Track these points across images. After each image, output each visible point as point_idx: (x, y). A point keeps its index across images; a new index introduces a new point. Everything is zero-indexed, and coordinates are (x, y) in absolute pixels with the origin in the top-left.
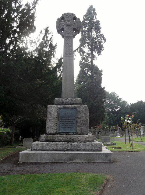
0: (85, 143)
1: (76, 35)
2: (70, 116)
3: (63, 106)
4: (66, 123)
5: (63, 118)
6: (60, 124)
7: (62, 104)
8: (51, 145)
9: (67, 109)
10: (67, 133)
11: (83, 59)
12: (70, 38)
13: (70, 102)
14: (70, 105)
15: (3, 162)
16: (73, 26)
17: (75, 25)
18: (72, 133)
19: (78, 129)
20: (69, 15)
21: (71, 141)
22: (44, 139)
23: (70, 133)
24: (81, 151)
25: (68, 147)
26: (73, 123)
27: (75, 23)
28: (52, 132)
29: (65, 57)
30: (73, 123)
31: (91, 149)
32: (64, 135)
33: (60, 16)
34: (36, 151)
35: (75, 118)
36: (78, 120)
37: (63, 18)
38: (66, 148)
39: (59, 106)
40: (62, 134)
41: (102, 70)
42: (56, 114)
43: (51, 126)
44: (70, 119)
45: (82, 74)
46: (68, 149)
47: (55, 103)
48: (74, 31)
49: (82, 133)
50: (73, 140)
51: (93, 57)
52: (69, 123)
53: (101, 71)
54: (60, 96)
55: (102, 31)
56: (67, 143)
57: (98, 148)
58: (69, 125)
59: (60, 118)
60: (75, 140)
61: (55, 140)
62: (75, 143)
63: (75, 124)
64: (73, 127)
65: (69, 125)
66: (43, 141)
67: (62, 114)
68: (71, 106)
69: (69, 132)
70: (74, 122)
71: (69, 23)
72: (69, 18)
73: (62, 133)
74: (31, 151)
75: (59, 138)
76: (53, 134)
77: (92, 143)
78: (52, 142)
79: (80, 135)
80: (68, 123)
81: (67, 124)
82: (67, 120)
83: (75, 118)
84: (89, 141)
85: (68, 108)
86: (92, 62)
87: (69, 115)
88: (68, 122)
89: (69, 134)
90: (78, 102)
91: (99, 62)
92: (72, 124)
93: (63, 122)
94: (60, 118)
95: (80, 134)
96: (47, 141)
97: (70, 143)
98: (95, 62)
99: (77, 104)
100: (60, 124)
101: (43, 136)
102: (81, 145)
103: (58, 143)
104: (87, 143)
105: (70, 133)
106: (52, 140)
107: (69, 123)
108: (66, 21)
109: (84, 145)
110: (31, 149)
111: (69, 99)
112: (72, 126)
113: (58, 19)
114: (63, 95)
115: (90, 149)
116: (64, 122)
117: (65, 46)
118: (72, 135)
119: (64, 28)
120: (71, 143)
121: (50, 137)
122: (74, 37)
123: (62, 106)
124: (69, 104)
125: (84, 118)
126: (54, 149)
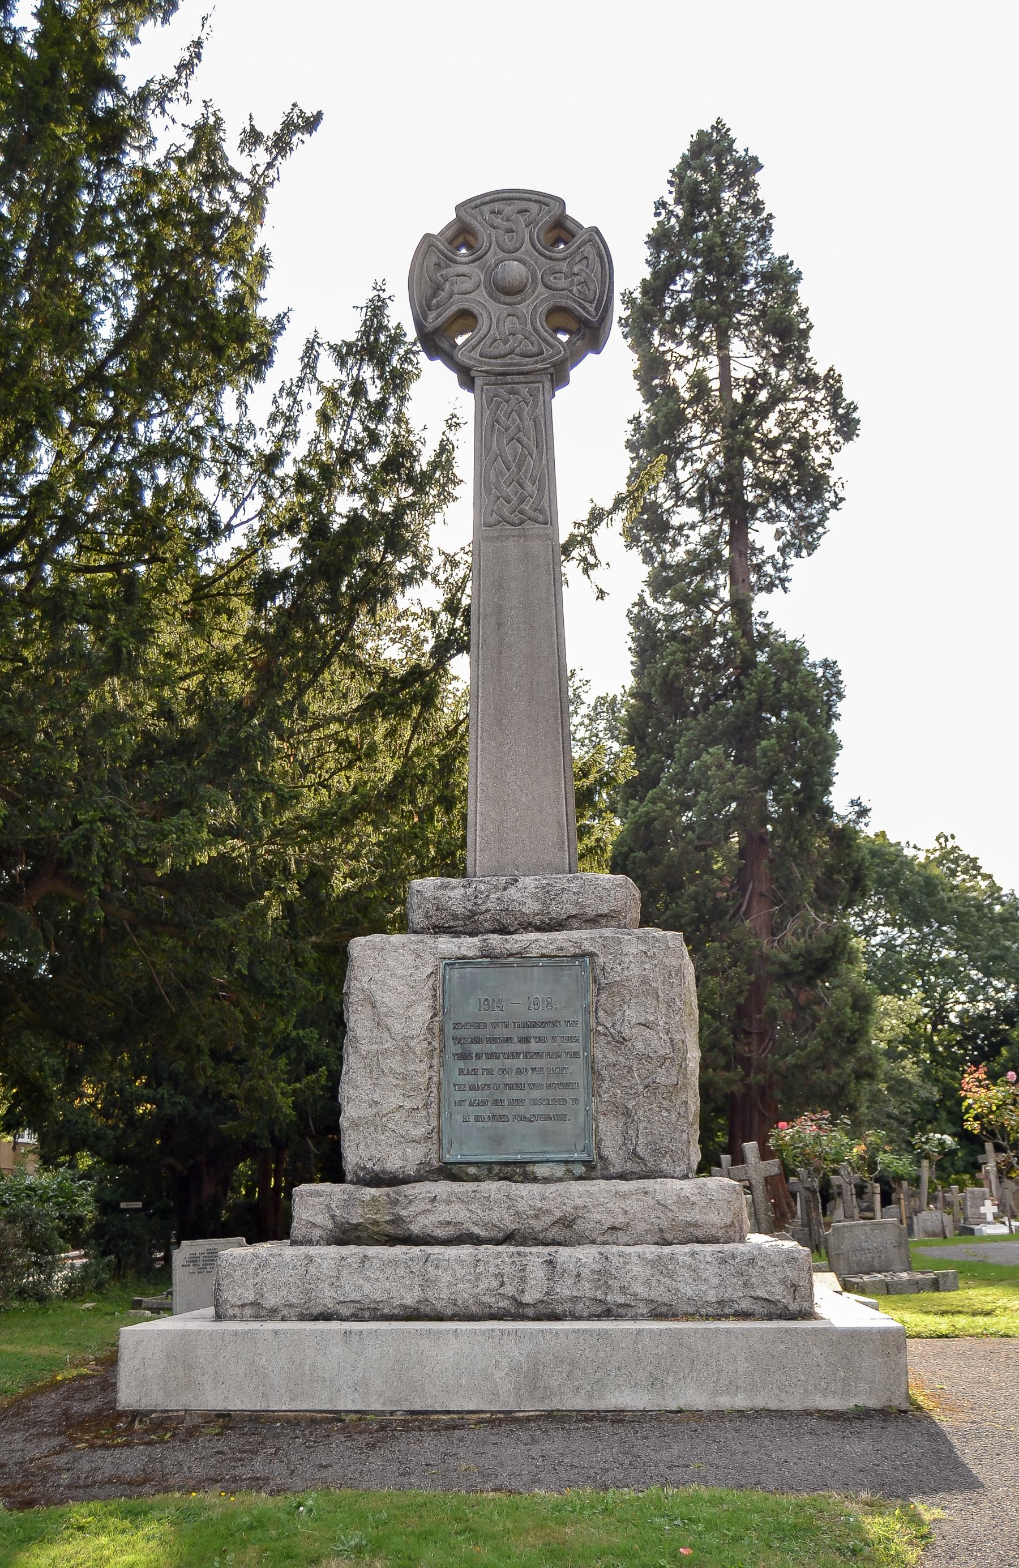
0: (667, 1250)
1: (575, 357)
2: (534, 1025)
3: (476, 940)
4: (511, 1087)
5: (476, 1041)
6: (458, 1096)
7: (465, 925)
8: (383, 1272)
9: (510, 965)
10: (515, 1171)
11: (659, 584)
12: (524, 390)
13: (536, 907)
14: (533, 936)
15: (16, 1411)
16: (547, 293)
17: (563, 283)
18: (559, 1171)
19: (609, 1129)
20: (508, 209)
21: (553, 1233)
22: (318, 1220)
23: (541, 1171)
24: (634, 1318)
25: (523, 1280)
26: (567, 1086)
27: (564, 266)
28: (393, 1164)
29: (487, 539)
30: (567, 1086)
31: (721, 1303)
32: (492, 1188)
33: (439, 218)
34: (256, 1317)
35: (573, 1039)
36: (603, 1052)
37: (462, 233)
38: (509, 1290)
39: (447, 945)
40: (476, 1179)
41: (848, 680)
42: (422, 1012)
43: (381, 1107)
44: (534, 1046)
45: (655, 711)
46: (527, 1299)
47: (417, 918)
48: (557, 330)
49: (636, 1169)
50: (567, 1222)
51: (749, 575)
52: (533, 1086)
53: (951, 856)
54: (450, 862)
55: (821, 354)
56: (512, 1249)
57: (779, 1293)
58: (534, 1102)
59: (458, 1040)
60: (580, 1226)
61: (415, 1228)
62: (586, 1254)
63: (581, 1094)
64: (562, 1117)
65: (534, 1102)
66: (317, 1233)
67: (470, 1010)
68: (544, 936)
69: (535, 1157)
70: (576, 1072)
71: (514, 270)
72: (509, 231)
73: (472, 1170)
74: (219, 1317)
75: (444, 1213)
76: (394, 1180)
77: (726, 1247)
78: (392, 1241)
79: (623, 1186)
80: (519, 1086)
81: (516, 1094)
82: (515, 1055)
83: (573, 1039)
84: (699, 1233)
85: (519, 954)
86: (740, 606)
87: (533, 1016)
88: (521, 1079)
89: (535, 1180)
90: (604, 909)
91: (810, 607)
92: (560, 1093)
93: (482, 1080)
94: (458, 1040)
95: (623, 1177)
96: (345, 1235)
97: (534, 1250)
98: (771, 609)
99: (594, 921)
100: (458, 1096)
101: (313, 1202)
102: (636, 1269)
103: (436, 1250)
104: (687, 1248)
105: (541, 1171)
106: (390, 1230)
107: (533, 1086)
108: (491, 259)
109: (656, 1263)
110: (217, 1313)
111: (528, 882)
112: (560, 1109)
113: (428, 242)
114: (475, 856)
115: (712, 1297)
116: (489, 1072)
117: (488, 449)
118: (560, 1180)
119: (476, 309)
120: (552, 1249)
121: (374, 1199)
122: (559, 377)
123: (468, 945)
124: (528, 926)
125: (657, 1043)
126: (409, 1301)
